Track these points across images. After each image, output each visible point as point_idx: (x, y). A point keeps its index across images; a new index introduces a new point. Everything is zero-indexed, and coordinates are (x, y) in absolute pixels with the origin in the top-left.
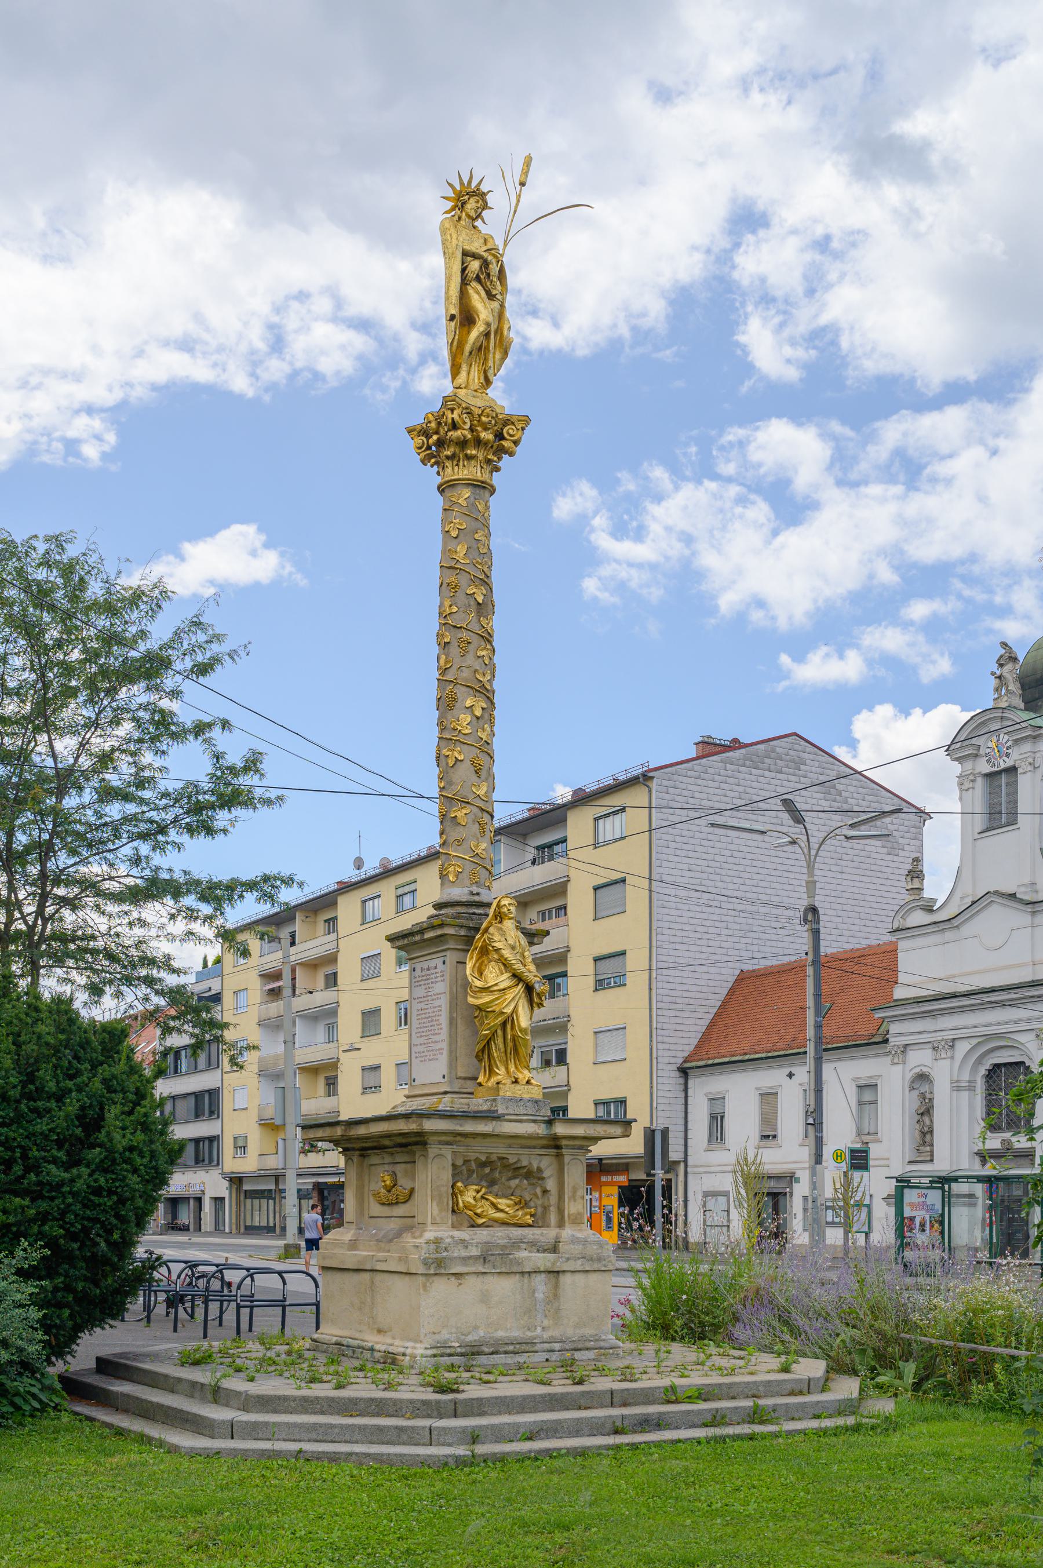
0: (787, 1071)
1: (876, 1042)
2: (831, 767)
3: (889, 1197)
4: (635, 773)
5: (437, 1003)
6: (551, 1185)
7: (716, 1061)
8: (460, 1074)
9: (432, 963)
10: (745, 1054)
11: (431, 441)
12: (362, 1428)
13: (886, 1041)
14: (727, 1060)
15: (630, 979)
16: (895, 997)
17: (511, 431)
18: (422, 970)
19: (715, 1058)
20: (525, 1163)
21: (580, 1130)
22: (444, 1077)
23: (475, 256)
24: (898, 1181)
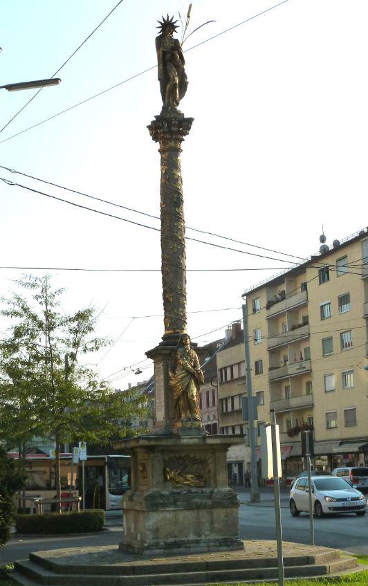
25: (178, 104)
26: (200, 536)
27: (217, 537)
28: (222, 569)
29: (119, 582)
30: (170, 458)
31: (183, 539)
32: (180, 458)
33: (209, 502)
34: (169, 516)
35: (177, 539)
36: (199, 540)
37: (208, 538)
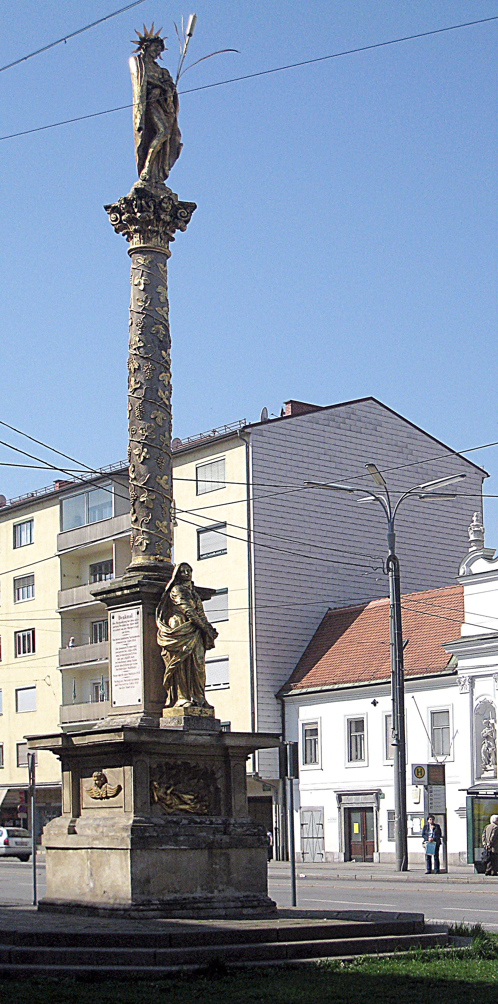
0: (372, 700)
1: (445, 675)
2: (404, 429)
3: (461, 809)
4: (234, 429)
5: (132, 644)
6: (220, 784)
7: (310, 690)
8: (152, 699)
9: (128, 613)
10: (335, 683)
11: (123, 217)
12: (118, 945)
13: (456, 673)
14: (319, 689)
15: (231, 615)
16: (463, 634)
17: (182, 214)
18: (120, 618)
19: (308, 687)
20: (202, 767)
21: (242, 742)
22: (139, 701)
23: (155, 87)
24: (468, 793)
25: (166, 177)
26: (212, 892)
27: (237, 894)
28: (339, 942)
29: (294, 967)
30: (160, 766)
31: (186, 895)
32: (175, 766)
33: (226, 838)
34: (165, 857)
35: (178, 895)
36: (212, 898)
37: (222, 895)
